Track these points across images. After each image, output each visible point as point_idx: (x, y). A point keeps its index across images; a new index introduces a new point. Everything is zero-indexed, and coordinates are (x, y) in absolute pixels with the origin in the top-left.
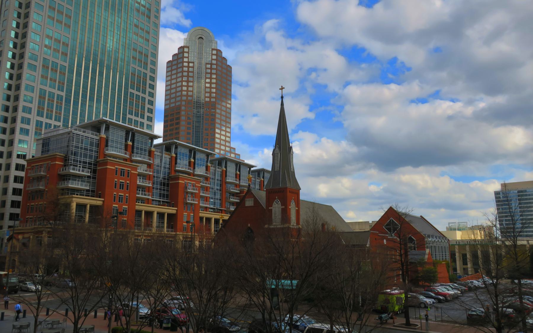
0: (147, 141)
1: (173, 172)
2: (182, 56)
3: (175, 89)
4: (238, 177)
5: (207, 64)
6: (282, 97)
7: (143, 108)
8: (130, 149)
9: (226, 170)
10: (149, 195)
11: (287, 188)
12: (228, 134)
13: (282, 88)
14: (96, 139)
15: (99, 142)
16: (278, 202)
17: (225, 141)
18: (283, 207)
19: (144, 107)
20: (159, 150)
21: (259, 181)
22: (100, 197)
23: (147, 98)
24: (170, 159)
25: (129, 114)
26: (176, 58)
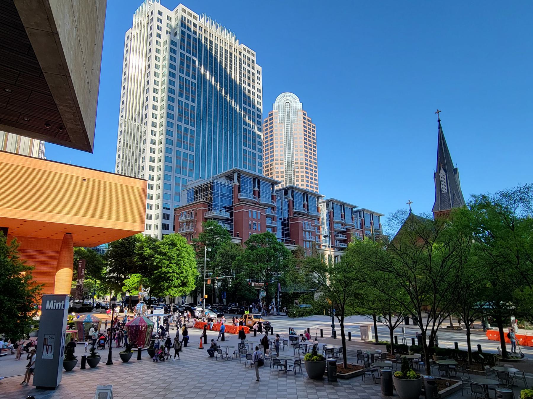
1: (292, 213)
6: (439, 121)
8: (257, 193)
13: (438, 113)
21: (360, 220)
22: (238, 236)
23: (257, 153)
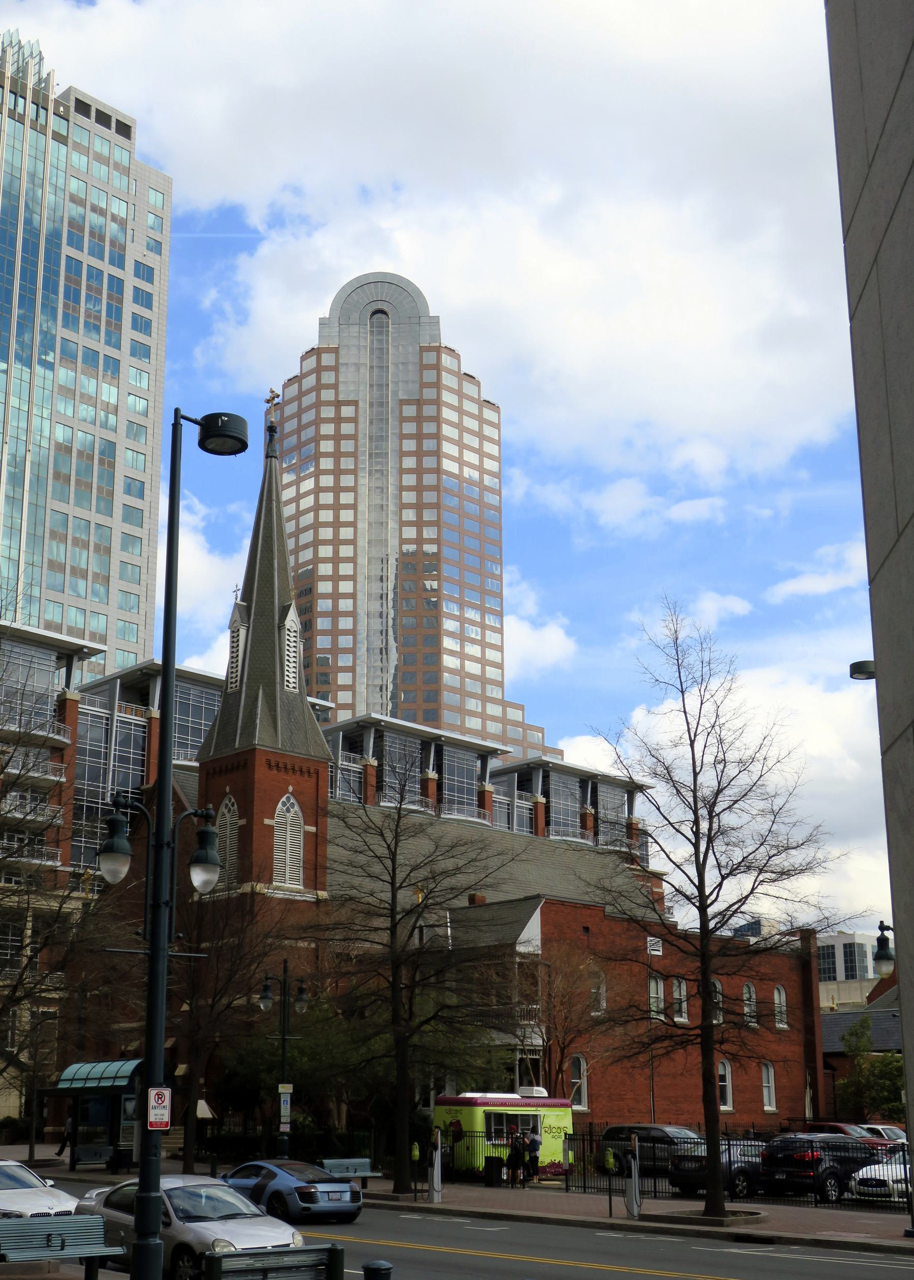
2: (314, 383)
3: (302, 508)
4: (590, 823)
5: (402, 402)
9: (548, 802)
10: (53, 857)
11: (255, 749)
12: (491, 655)
14: (136, 725)
15: (144, 732)
16: (233, 805)
17: (483, 680)
18: (243, 822)
20: (501, 789)
24: (530, 809)
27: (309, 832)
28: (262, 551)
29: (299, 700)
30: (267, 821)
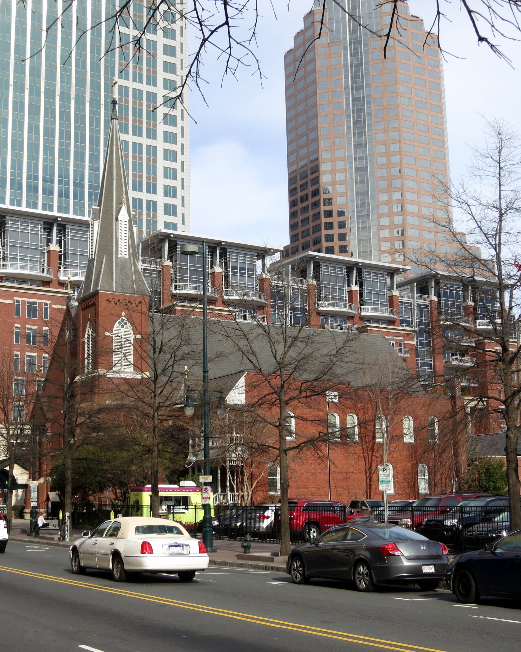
0: (384, 280)
7: (152, 169)
19: (155, 168)
25: (134, 189)
26: (301, 39)
27: (138, 339)
28: (107, 176)
29: (128, 262)
30: (107, 334)
